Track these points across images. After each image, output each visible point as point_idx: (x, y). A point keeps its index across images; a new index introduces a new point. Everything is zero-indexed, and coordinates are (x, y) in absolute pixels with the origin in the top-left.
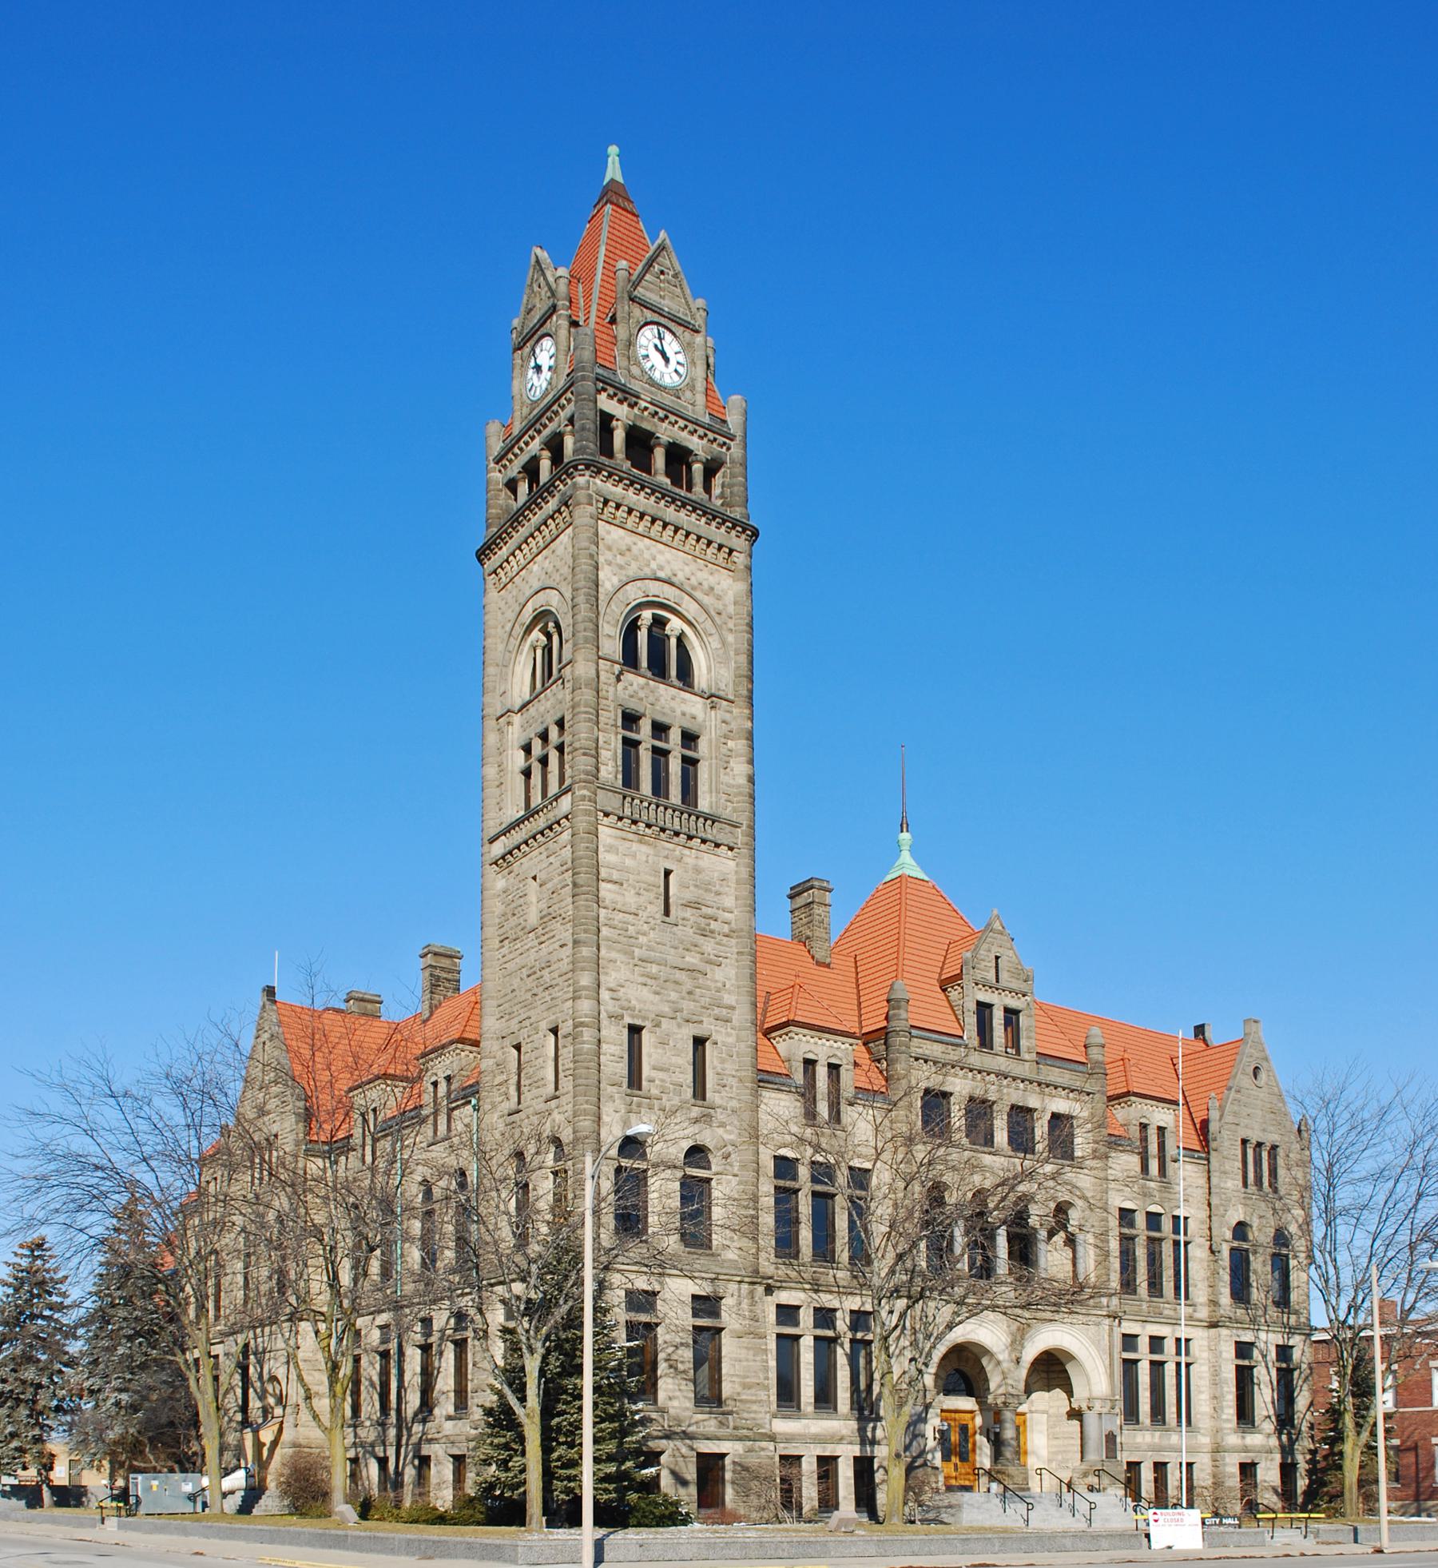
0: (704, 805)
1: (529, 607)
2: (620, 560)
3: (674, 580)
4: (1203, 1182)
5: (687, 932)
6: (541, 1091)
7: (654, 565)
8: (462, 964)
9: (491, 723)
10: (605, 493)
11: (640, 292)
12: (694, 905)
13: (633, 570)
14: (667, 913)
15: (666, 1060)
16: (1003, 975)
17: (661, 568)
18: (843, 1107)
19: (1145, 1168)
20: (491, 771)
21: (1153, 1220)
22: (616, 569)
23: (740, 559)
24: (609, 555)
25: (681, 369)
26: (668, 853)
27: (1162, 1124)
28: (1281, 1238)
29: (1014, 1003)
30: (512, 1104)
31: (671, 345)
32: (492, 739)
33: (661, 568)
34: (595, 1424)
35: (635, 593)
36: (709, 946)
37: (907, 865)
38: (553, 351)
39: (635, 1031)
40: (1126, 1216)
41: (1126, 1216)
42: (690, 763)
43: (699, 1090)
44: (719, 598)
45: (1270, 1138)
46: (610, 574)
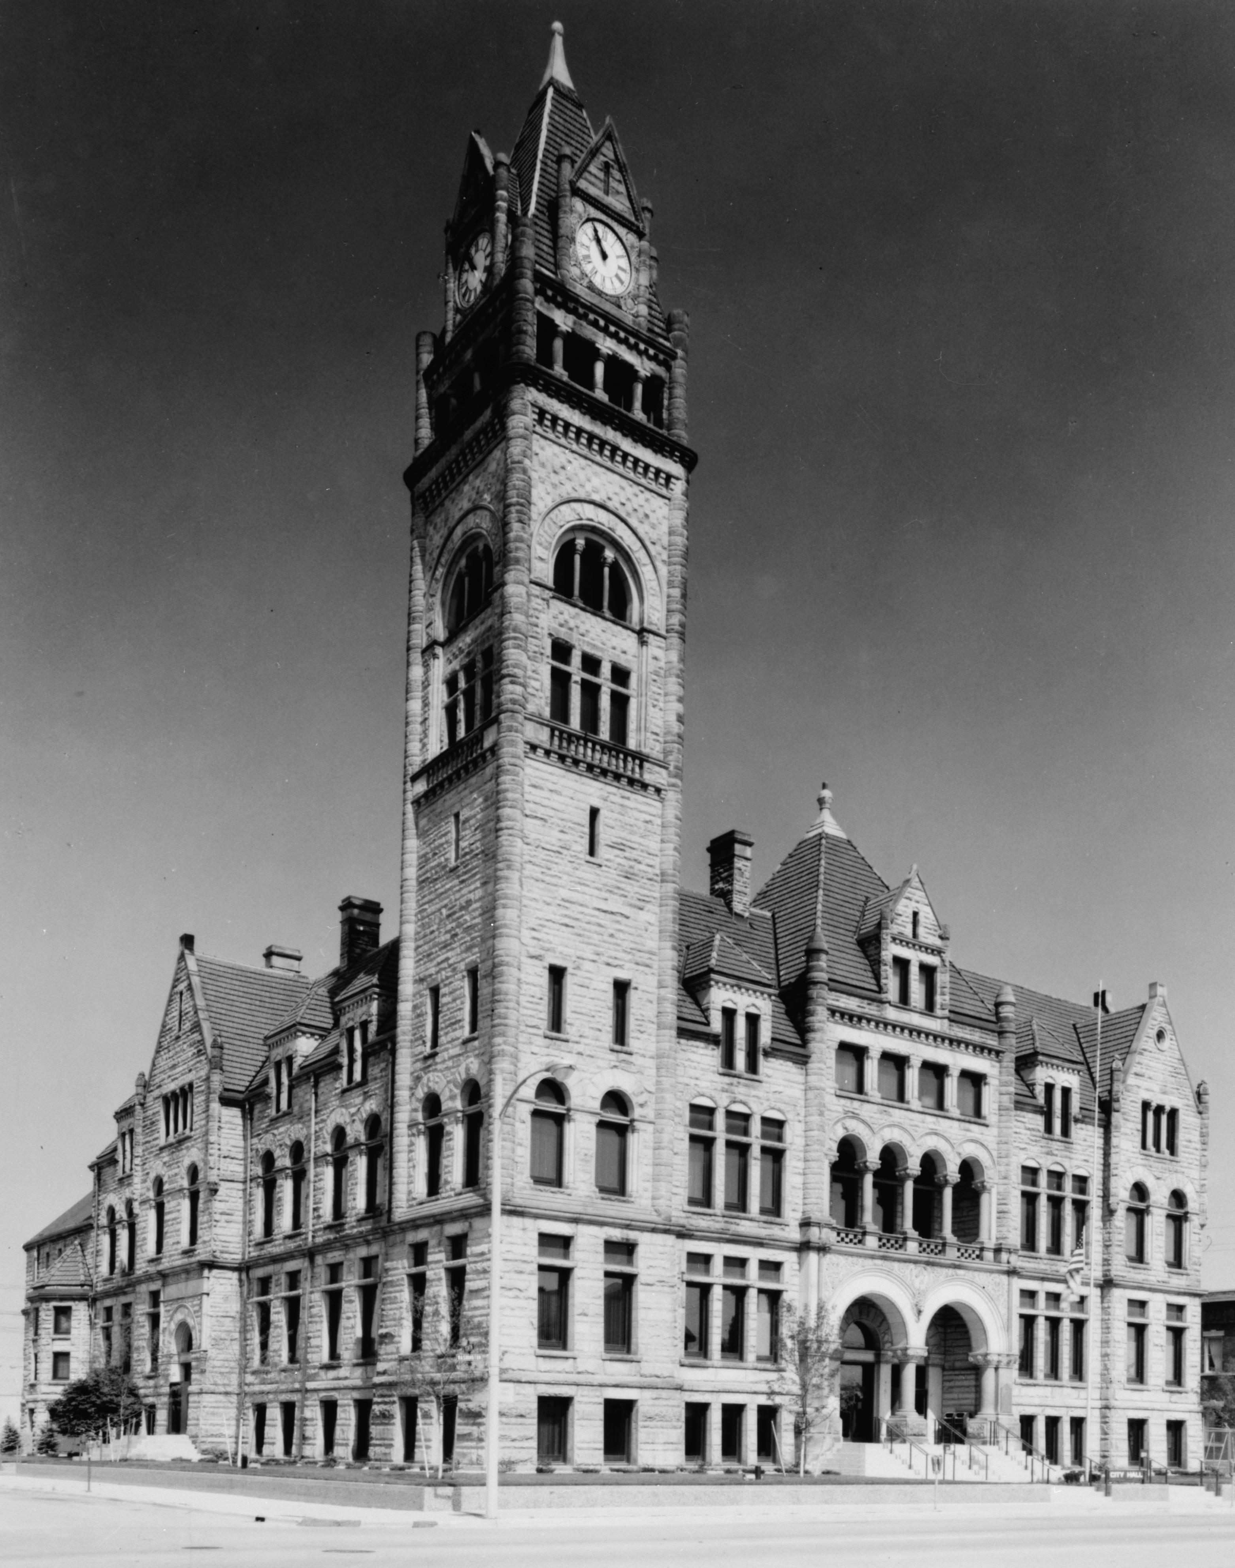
0: (632, 743)
1: (459, 531)
2: (554, 478)
3: (609, 504)
4: (1100, 1142)
5: (611, 876)
6: (458, 1033)
7: (588, 487)
8: (383, 918)
9: (416, 657)
10: (541, 403)
11: (582, 184)
12: (619, 846)
13: (567, 491)
14: (592, 852)
15: (588, 1002)
16: (921, 930)
17: (596, 491)
18: (761, 1058)
19: (1049, 1129)
20: (415, 706)
21: (1057, 1177)
22: (550, 489)
23: (679, 487)
24: (542, 472)
25: (623, 276)
26: (595, 791)
27: (1067, 1085)
28: (1178, 1197)
29: (932, 960)
30: (428, 1050)
31: (610, 242)
32: (417, 672)
33: (596, 491)
34: (424, 1025)
35: (569, 516)
36: (632, 888)
37: (831, 827)
38: (488, 250)
39: (557, 974)
40: (1030, 1173)
41: (1030, 1173)
42: (620, 703)
43: (620, 1036)
44: (653, 527)
45: (1168, 1102)
46: (543, 494)
